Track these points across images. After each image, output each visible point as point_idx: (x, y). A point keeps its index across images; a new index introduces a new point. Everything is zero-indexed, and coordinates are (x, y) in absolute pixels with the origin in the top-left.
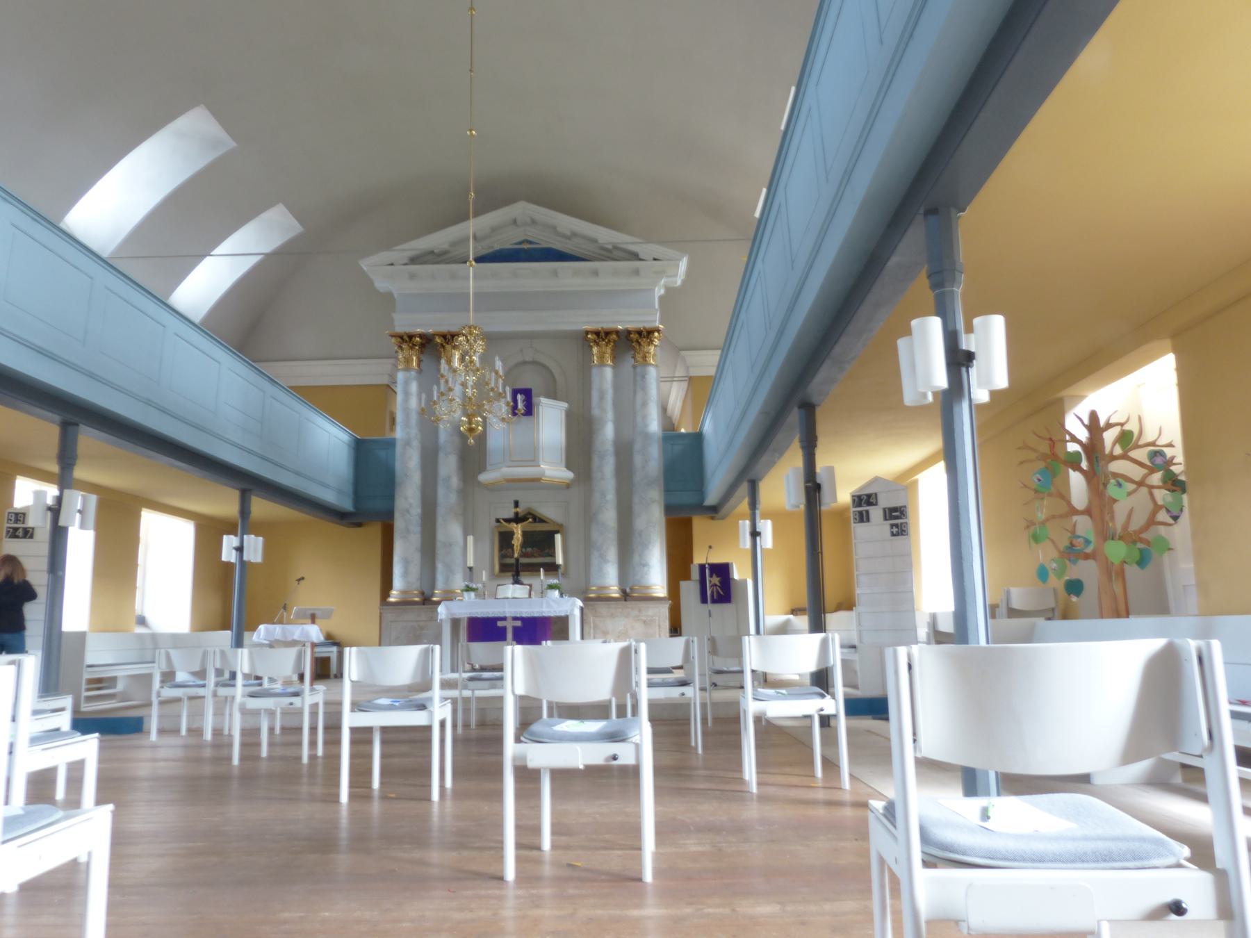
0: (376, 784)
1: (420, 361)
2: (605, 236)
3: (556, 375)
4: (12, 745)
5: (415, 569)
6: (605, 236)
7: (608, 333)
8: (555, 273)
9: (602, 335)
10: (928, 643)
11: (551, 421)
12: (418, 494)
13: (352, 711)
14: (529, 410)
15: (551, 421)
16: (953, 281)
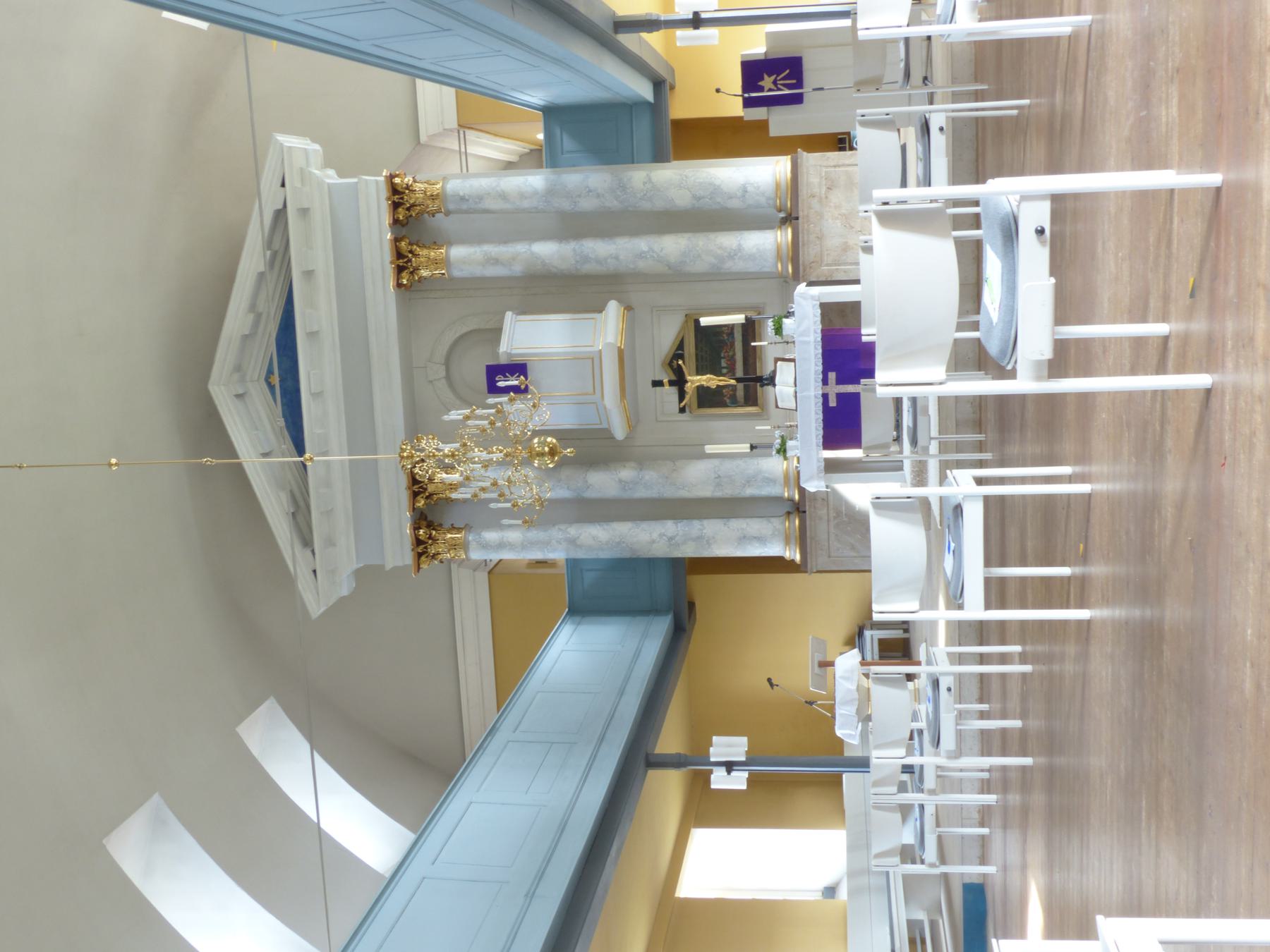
1: (453, 529)
4: (822, 89)
5: (754, 526)
6: (252, 261)
7: (399, 255)
9: (402, 263)
11: (532, 336)
12: (645, 525)
14: (519, 369)
15: (532, 336)
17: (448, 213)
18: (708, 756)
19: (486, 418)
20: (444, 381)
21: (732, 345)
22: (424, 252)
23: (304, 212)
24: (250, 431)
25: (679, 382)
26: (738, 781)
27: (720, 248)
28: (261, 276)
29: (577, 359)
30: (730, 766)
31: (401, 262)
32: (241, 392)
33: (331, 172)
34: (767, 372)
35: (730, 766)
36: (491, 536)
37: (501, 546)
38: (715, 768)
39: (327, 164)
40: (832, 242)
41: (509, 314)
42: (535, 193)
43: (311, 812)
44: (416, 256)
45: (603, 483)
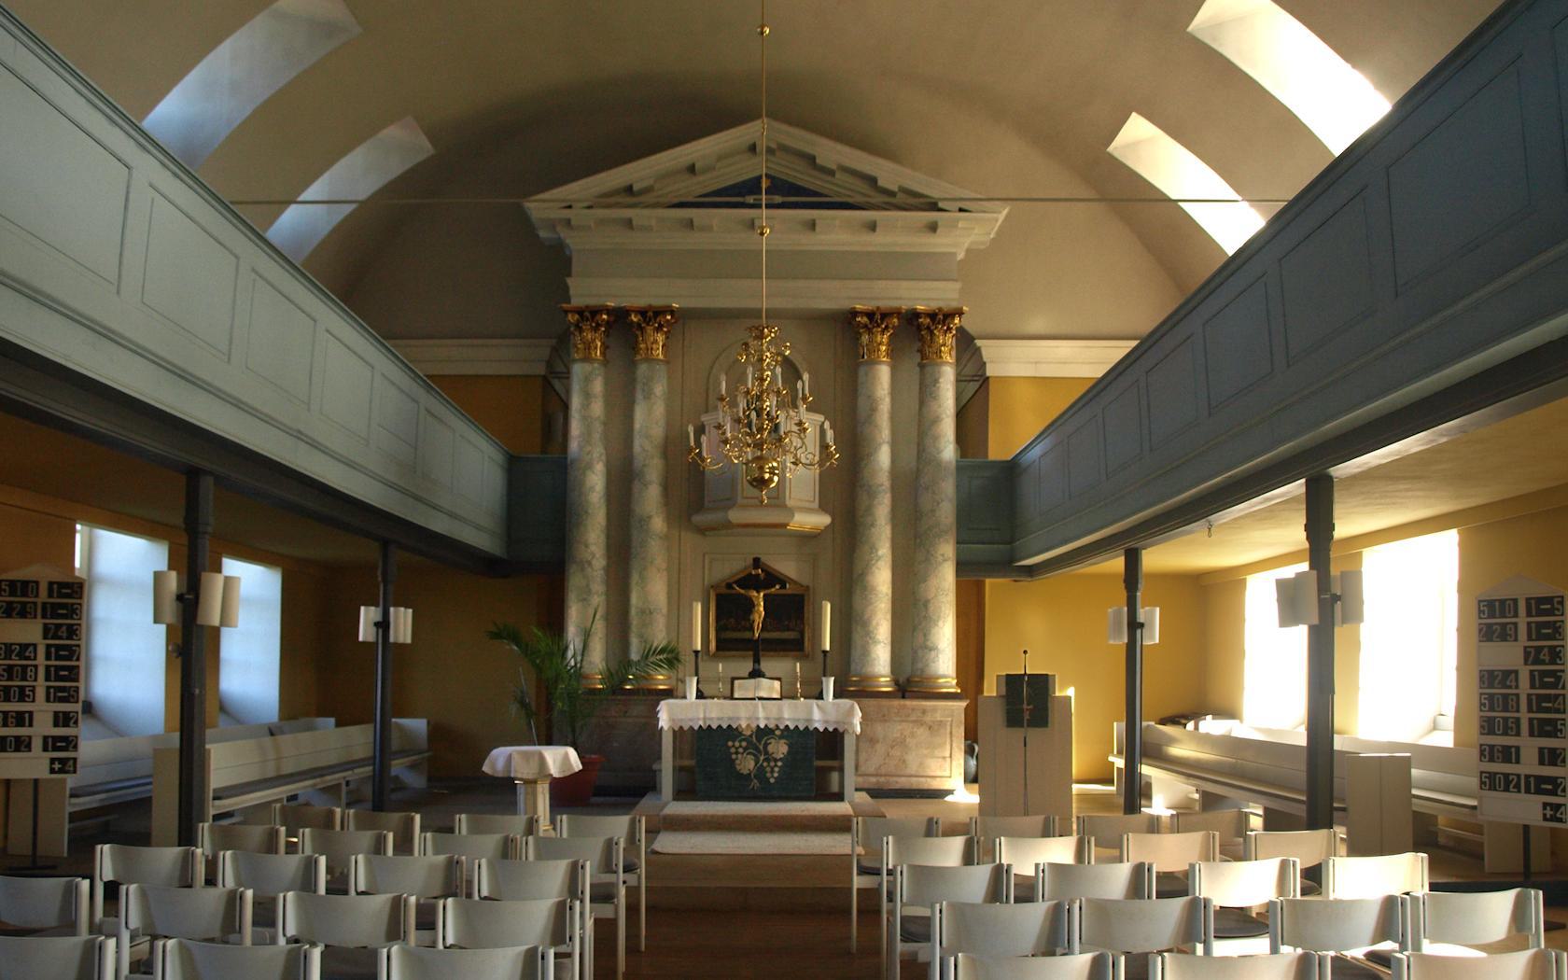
1: (605, 347)
5: (668, 627)
8: (812, 225)
9: (877, 318)
10: (1146, 954)
12: (602, 539)
17: (922, 366)
18: (397, 605)
21: (778, 630)
25: (749, 582)
26: (365, 632)
30: (383, 625)
31: (878, 316)
34: (766, 665)
35: (383, 625)
36: (598, 386)
37: (587, 396)
38: (380, 609)
43: (308, 195)
44: (883, 333)
45: (650, 499)
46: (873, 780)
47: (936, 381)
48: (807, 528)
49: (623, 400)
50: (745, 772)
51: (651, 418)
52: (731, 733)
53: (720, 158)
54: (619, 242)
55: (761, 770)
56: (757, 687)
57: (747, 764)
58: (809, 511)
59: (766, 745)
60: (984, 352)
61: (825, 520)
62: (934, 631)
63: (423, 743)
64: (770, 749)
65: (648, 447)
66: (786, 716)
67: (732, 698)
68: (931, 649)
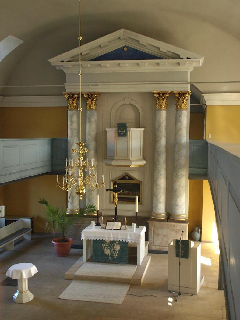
0: (58, 181)
2: (164, 47)
3: (140, 111)
4: (180, 265)
6: (164, 47)
7: (163, 94)
9: (161, 95)
11: (136, 136)
13: (96, 225)
14: (125, 135)
15: (136, 136)
16: (93, 250)
17: (177, 111)
19: (92, 169)
20: (124, 103)
22: (164, 101)
23: (179, 64)
24: (108, 42)
27: (160, 197)
28: (159, 48)
29: (127, 151)
32: (121, 38)
33: (192, 70)
37: (72, 122)
39: (195, 68)
40: (160, 232)
41: (143, 129)
42: (181, 140)
46: (158, 247)
47: (180, 116)
48: (138, 166)
49: (84, 121)
50: (107, 254)
51: (91, 129)
52: (102, 242)
53: (109, 42)
54: (82, 71)
55: (112, 254)
56: (113, 225)
57: (107, 252)
58: (139, 160)
59: (113, 246)
60: (205, 97)
61: (144, 162)
62: (178, 199)
63: (30, 226)
64: (115, 247)
65: (90, 139)
66: (119, 237)
67: (105, 229)
68: (177, 206)
